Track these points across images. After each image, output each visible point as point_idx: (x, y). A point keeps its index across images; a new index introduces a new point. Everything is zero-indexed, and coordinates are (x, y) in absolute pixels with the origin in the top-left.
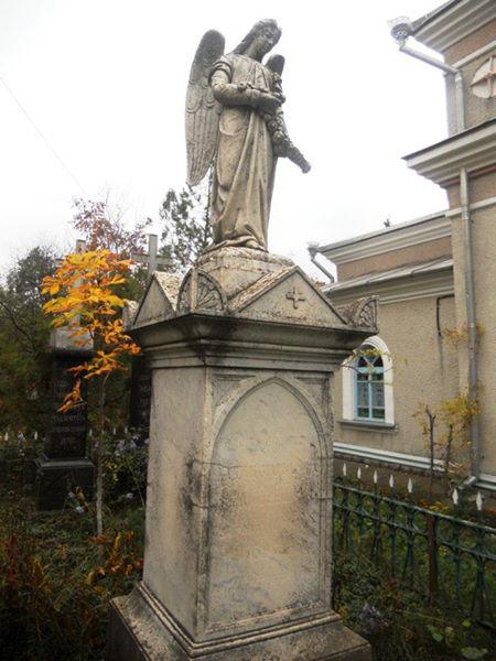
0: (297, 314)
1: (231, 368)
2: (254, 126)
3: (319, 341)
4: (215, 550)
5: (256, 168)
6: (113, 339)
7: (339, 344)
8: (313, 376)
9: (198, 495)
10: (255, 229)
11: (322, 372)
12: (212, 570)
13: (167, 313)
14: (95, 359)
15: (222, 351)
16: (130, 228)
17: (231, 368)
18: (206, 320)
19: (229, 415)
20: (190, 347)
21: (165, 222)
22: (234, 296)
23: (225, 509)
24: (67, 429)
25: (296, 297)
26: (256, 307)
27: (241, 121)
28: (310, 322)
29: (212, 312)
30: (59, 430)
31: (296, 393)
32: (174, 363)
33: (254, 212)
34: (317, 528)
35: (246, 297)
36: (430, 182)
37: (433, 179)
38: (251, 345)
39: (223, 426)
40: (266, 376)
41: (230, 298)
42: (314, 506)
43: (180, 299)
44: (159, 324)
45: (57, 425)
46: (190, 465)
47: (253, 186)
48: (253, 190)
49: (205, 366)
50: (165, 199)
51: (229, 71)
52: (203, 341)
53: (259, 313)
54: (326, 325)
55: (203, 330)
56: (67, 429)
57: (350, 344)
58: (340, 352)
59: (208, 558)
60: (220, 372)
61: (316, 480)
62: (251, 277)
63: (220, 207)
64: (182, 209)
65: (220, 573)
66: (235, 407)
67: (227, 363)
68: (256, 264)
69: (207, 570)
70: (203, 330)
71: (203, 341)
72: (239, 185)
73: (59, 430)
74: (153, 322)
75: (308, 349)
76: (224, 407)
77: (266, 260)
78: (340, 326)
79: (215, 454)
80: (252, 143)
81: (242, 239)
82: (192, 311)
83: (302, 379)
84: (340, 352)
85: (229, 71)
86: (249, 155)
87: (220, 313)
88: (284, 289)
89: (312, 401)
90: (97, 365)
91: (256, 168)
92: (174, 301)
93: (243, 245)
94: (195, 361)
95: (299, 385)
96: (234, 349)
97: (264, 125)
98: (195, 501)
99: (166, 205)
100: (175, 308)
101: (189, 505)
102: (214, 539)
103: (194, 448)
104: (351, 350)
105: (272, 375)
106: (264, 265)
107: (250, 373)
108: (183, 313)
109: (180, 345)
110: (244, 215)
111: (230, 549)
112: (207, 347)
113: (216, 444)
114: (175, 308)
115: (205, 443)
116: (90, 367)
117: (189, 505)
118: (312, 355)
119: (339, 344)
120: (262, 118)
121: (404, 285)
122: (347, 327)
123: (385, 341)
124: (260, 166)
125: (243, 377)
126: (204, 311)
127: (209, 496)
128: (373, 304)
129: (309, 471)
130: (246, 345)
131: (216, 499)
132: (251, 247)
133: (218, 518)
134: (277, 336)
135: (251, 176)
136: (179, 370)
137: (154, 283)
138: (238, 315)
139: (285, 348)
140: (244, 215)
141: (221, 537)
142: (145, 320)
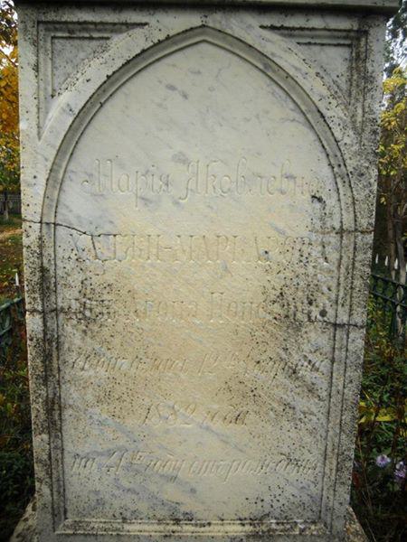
4: (71, 394)
8: (316, 22)
23: (87, 318)
31: (267, 66)
76: (73, 97)
89: (316, 88)
105: (274, 59)
129: (304, 260)
131: (67, 297)
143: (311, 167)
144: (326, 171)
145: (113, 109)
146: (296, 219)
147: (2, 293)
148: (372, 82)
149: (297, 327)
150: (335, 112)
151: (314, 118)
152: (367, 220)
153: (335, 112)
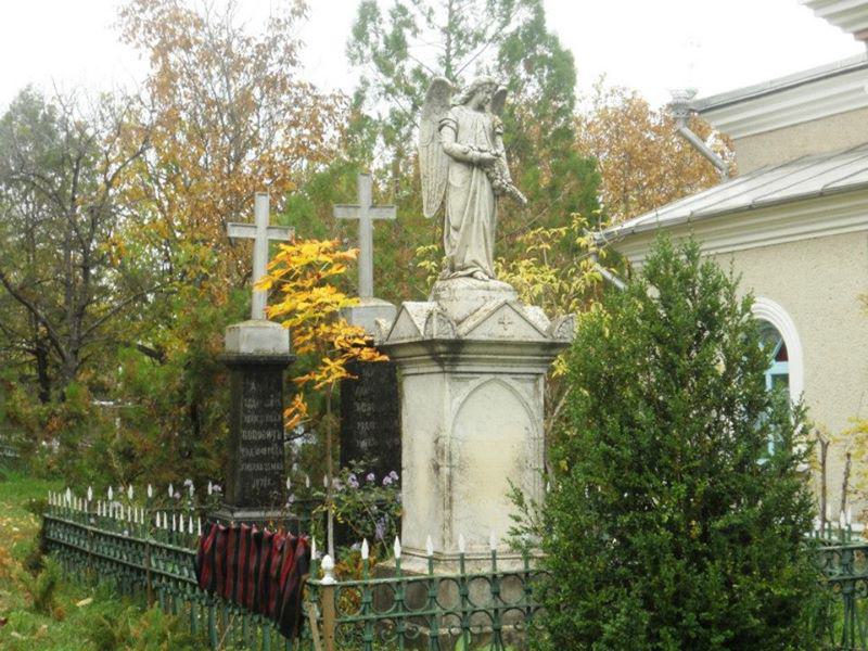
0: (507, 333)
1: (461, 372)
2: (478, 177)
3: (525, 351)
4: (456, 496)
5: (479, 212)
6: (343, 344)
7: (542, 352)
8: (524, 377)
9: (442, 458)
10: (480, 261)
11: (533, 374)
12: (454, 507)
13: (416, 336)
14: (321, 368)
15: (455, 361)
16: (259, 32)
17: (461, 372)
18: (443, 342)
19: (462, 405)
20: (434, 359)
21: (358, 70)
22: (463, 321)
23: (461, 469)
24: (259, 467)
25: (506, 322)
26: (476, 331)
27: (467, 173)
28: (517, 338)
29: (447, 337)
30: (249, 467)
31: (511, 389)
32: (421, 371)
33: (480, 247)
34: (532, 490)
35: (470, 323)
36: (839, 29)
37: (844, 26)
38: (475, 356)
39: (458, 413)
40: (488, 377)
41: (459, 323)
42: (529, 474)
43: (426, 328)
44: (411, 343)
45: (247, 460)
46: (436, 442)
47: (478, 227)
48: (478, 231)
49: (444, 372)
50: (356, 17)
51: (454, 125)
52: (442, 356)
53: (480, 335)
54: (530, 340)
55: (441, 348)
56: (259, 467)
57: (553, 352)
58: (545, 358)
59: (451, 499)
60: (455, 375)
61: (531, 455)
62: (476, 305)
63: (453, 244)
64: (397, 45)
65: (459, 511)
66: (465, 401)
67: (458, 369)
68: (481, 293)
69: (450, 507)
70: (441, 348)
71: (442, 356)
72: (467, 227)
73: (249, 467)
74: (405, 341)
75: (519, 357)
76: (459, 399)
77: (488, 289)
78: (542, 339)
79: (453, 431)
80: (475, 193)
81: (470, 271)
82: (435, 337)
83: (517, 379)
84: (545, 358)
85: (454, 125)
86: (473, 203)
87: (452, 337)
88: (497, 317)
89: (526, 396)
90: (324, 375)
91: (479, 212)
92: (422, 328)
93: (471, 275)
94: (437, 369)
95: (514, 383)
96: (464, 360)
97: (485, 175)
98: (440, 464)
99: (360, 33)
100: (422, 333)
101: (437, 468)
102: (454, 488)
103: (439, 428)
104: (556, 356)
105: (492, 376)
106: (486, 293)
107: (475, 375)
108: (429, 338)
109: (426, 357)
110: (471, 252)
111: (466, 497)
112: (446, 359)
113: (454, 425)
114: (422, 333)
115: (446, 423)
116: (318, 378)
117: (437, 468)
118: (521, 361)
119: (542, 352)
120: (482, 170)
121: (848, 204)
122: (548, 340)
123: (786, 307)
124: (482, 210)
125: (471, 378)
126: (443, 337)
127: (450, 459)
128: (570, 321)
129: (524, 448)
130: (471, 356)
131: (455, 462)
132: (476, 278)
133: (456, 474)
134: (494, 349)
135: (475, 221)
136: (425, 376)
137: (404, 311)
138: (464, 338)
139: (500, 357)
140: (471, 252)
141: (460, 488)
142: (394, 340)
143: (521, 416)
144: (529, 420)
145: (469, 402)
146: (521, 435)
147: (296, 2)
148: (342, 286)
149: (523, 470)
150: (531, 403)
151: (525, 405)
152: (541, 435)
153: (531, 403)
